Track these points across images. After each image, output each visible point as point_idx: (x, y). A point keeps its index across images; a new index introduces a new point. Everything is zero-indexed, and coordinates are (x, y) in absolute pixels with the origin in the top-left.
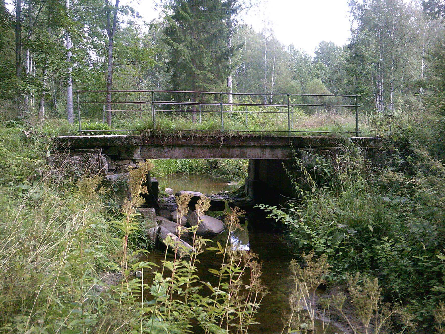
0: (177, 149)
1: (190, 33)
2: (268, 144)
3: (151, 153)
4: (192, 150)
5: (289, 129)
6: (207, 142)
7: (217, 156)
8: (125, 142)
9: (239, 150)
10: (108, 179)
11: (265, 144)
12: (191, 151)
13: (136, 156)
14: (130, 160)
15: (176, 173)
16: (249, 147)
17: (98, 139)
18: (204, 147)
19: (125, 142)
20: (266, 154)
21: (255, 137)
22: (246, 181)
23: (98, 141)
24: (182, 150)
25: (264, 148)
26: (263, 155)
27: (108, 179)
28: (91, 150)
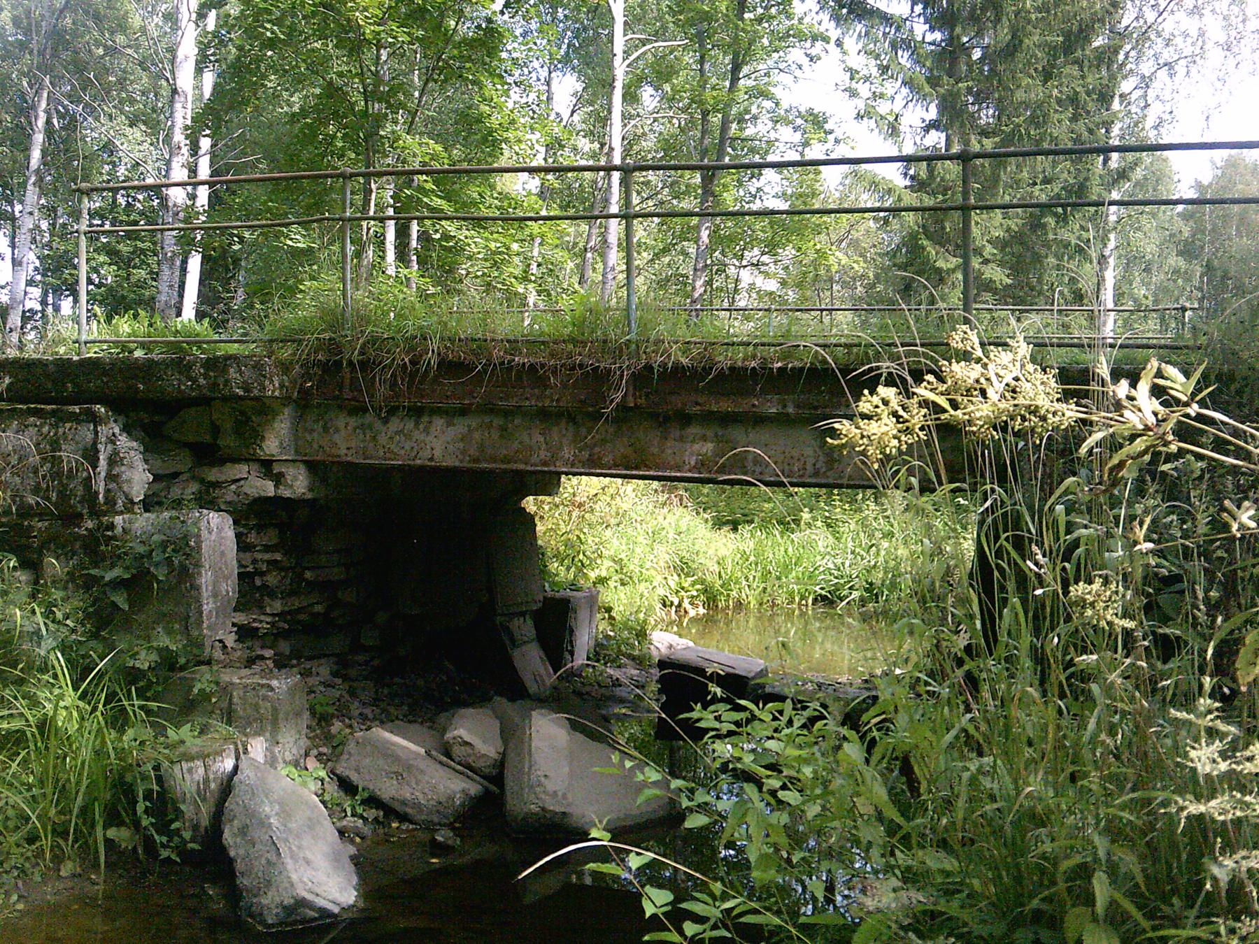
0: (439, 422)
1: (784, 194)
3: (336, 438)
4: (504, 429)
6: (556, 395)
7: (607, 459)
8: (202, 381)
9: (710, 433)
10: (119, 530)
12: (495, 434)
13: (272, 446)
15: (815, 600)
16: (759, 420)
17: (646, 466)
18: (544, 415)
19: (202, 381)
23: (105, 373)
24: (460, 426)
27: (119, 530)
28: (71, 408)
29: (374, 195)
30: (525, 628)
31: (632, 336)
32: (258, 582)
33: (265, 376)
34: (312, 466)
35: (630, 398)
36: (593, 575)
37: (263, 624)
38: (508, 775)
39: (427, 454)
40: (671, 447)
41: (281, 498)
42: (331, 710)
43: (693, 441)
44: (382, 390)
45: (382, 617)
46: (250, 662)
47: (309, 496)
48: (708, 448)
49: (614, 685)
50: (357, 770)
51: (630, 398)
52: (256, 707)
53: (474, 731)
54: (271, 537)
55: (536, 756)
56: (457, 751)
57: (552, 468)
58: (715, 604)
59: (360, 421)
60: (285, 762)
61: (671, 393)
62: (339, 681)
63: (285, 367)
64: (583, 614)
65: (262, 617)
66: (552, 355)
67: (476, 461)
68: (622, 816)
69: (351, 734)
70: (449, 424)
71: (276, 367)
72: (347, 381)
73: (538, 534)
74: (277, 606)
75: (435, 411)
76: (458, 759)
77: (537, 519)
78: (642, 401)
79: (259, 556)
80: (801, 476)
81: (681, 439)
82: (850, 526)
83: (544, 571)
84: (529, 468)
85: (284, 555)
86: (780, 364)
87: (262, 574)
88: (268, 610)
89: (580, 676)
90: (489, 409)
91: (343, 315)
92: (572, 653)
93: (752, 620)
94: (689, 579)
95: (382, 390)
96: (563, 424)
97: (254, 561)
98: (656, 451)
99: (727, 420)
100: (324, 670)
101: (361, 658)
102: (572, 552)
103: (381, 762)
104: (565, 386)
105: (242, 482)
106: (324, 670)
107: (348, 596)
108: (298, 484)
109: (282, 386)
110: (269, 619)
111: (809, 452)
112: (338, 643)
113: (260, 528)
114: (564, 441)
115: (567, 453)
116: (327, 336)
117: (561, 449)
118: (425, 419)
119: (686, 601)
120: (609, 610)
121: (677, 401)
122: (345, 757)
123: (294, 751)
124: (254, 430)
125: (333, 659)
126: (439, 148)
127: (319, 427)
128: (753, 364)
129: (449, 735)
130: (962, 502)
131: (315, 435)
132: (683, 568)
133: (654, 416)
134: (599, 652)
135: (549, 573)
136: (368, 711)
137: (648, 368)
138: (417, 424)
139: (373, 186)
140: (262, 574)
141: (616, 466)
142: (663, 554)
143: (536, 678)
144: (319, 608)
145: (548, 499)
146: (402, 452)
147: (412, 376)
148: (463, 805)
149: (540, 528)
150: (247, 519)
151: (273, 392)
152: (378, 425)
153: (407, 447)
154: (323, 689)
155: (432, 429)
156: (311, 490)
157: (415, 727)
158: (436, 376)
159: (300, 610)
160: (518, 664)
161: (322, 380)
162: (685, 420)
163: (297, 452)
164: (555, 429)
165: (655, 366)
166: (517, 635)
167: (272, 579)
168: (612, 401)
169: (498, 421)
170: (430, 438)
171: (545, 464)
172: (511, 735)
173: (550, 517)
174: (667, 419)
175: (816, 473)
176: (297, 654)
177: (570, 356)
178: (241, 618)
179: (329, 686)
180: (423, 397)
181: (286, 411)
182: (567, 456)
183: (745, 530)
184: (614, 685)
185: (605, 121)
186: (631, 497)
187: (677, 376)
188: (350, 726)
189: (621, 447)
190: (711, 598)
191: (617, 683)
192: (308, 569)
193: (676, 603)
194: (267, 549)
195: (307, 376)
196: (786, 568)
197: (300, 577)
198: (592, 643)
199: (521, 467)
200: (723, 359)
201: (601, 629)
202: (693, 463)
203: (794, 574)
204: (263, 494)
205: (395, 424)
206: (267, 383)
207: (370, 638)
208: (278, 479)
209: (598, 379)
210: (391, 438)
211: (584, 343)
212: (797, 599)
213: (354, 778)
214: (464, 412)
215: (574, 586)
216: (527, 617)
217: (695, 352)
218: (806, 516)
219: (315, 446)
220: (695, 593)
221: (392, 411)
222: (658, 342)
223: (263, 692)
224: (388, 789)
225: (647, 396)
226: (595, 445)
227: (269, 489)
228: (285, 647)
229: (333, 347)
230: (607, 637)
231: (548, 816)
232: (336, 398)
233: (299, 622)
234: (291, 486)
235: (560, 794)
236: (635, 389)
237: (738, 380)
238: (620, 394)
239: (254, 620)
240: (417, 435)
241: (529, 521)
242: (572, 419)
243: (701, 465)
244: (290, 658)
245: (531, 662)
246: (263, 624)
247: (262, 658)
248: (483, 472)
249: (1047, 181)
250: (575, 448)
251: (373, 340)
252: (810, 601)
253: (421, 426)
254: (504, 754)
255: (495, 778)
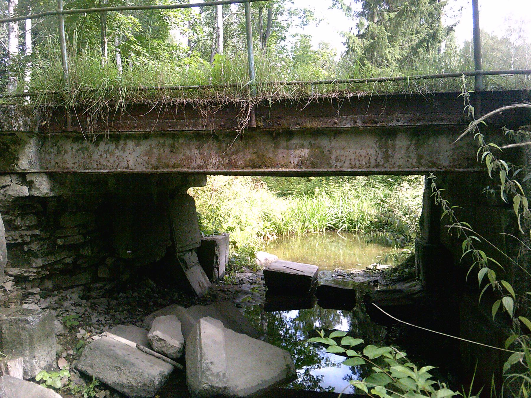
0: (131, 144)
2: (398, 121)
4: (173, 146)
5: (478, 64)
9: (306, 143)
11: (389, 121)
12: (167, 151)
14: (14, 178)
15: (326, 229)
16: (337, 133)
17: (266, 166)
18: (198, 136)
20: (396, 156)
21: (354, 98)
22: (417, 248)
24: (145, 146)
25: (388, 134)
26: (386, 157)
29: (106, 45)
30: (192, 258)
31: (253, 81)
32: (26, 248)
33: (11, 118)
34: (51, 176)
35: (254, 122)
36: (225, 226)
37: (32, 273)
38: (187, 357)
39: (124, 164)
40: (281, 153)
41: (33, 197)
42: (76, 323)
43: (296, 148)
44: (92, 125)
45: (109, 261)
46: (25, 296)
47: (52, 194)
48: (305, 152)
49: (240, 283)
50: (91, 366)
51: (254, 122)
52: (18, 335)
53: (165, 331)
54: (32, 220)
55: (205, 350)
56: (155, 344)
57: (205, 170)
58: (281, 235)
59: (81, 146)
60: (40, 368)
61: (280, 118)
62: (84, 301)
63: (27, 112)
64: (222, 248)
65: (31, 270)
66: (202, 97)
67: (157, 167)
68: (260, 382)
69: (90, 337)
70: (138, 145)
71: (19, 111)
72: (69, 121)
73: (197, 206)
74: (39, 262)
75: (128, 137)
76: (156, 349)
77: (195, 198)
78: (261, 124)
79: (24, 233)
80: (368, 168)
81: (288, 148)
82: (337, 194)
83: (200, 225)
84: (190, 171)
85: (41, 231)
86: (352, 95)
87: (27, 243)
88: (34, 265)
89: (223, 280)
90: (163, 134)
91: (63, 76)
92: (218, 268)
93: (299, 240)
94: (269, 223)
95: (92, 125)
96: (211, 142)
97: (22, 236)
98: (271, 156)
99: (317, 133)
100: (75, 295)
101: (99, 285)
102: (214, 215)
103: (106, 360)
104: (211, 117)
105: (8, 187)
106: (75, 295)
107: (86, 252)
108: (43, 187)
109: (25, 124)
110: (35, 270)
111: (371, 152)
112: (84, 278)
113: (23, 216)
114: (212, 152)
115: (214, 160)
116: (53, 91)
117: (210, 157)
118: (122, 142)
119: (268, 233)
120: (234, 243)
121: (285, 123)
122: (83, 358)
123: (48, 359)
124: (12, 154)
125: (81, 288)
126: (137, 20)
127: (54, 150)
128: (334, 95)
129: (150, 335)
130: (391, 180)
131: (52, 156)
132: (266, 218)
133: (270, 133)
134: (231, 267)
135: (204, 227)
136: (102, 319)
137: (265, 102)
138: (117, 147)
139: (106, 40)
140: (27, 243)
141: (246, 166)
142: (257, 212)
143: (200, 284)
144: (68, 260)
145: (201, 188)
146: (109, 164)
147: (111, 113)
148: (160, 382)
149: (197, 203)
150: (14, 210)
151: (19, 127)
152: (92, 147)
153: (112, 161)
154: (73, 308)
155: (127, 149)
156: (52, 190)
157: (131, 328)
158: (126, 114)
159: (56, 262)
160: (189, 278)
161: (52, 119)
162: (289, 134)
163: (41, 167)
164: (206, 145)
165: (270, 100)
166: (187, 260)
167: (35, 247)
168: (242, 125)
169: (169, 142)
170: (126, 154)
171: (200, 167)
172: (189, 332)
173: (202, 197)
174: (278, 135)
175: (377, 166)
176: (57, 288)
177: (212, 96)
178: (16, 271)
179: (79, 305)
180: (119, 128)
181: (32, 141)
182: (214, 162)
183: (290, 197)
184: (240, 283)
185: (215, 18)
186: (241, 185)
187: (284, 106)
188: (90, 332)
189: (249, 155)
190: (280, 233)
191: (242, 282)
192: (59, 238)
193: (264, 235)
194: (29, 228)
195: (43, 118)
196: (313, 215)
197: (55, 243)
198: (227, 261)
199: (185, 170)
200: (312, 92)
201: (231, 252)
202: (296, 163)
203: (316, 217)
204: (21, 195)
205: (103, 147)
206: (13, 121)
207: (103, 273)
208: (31, 185)
209: (232, 110)
210: (101, 155)
211: (222, 87)
212: (318, 229)
213: (90, 371)
214: (146, 136)
215: (216, 233)
216: (194, 252)
217: (295, 88)
218: (317, 190)
219: (53, 163)
220: (272, 229)
221: (100, 138)
222: (271, 84)
223: (22, 324)
224: (112, 378)
225: (264, 120)
226: (232, 154)
227: (25, 191)
228: (49, 284)
229: (59, 98)
230: (235, 257)
231: (215, 390)
232: (64, 131)
233: (56, 270)
234: (39, 189)
235: (221, 374)
236: (256, 116)
237: (323, 106)
238: (248, 119)
239: (25, 272)
240: (118, 153)
241: (191, 200)
242: (216, 138)
243: (301, 163)
244: (52, 291)
245: (197, 277)
246: (32, 273)
247: (32, 294)
248: (162, 175)
249: (417, 33)
250: (219, 156)
251: (83, 92)
252: (324, 230)
253: (120, 147)
254: (184, 346)
255: (180, 362)
